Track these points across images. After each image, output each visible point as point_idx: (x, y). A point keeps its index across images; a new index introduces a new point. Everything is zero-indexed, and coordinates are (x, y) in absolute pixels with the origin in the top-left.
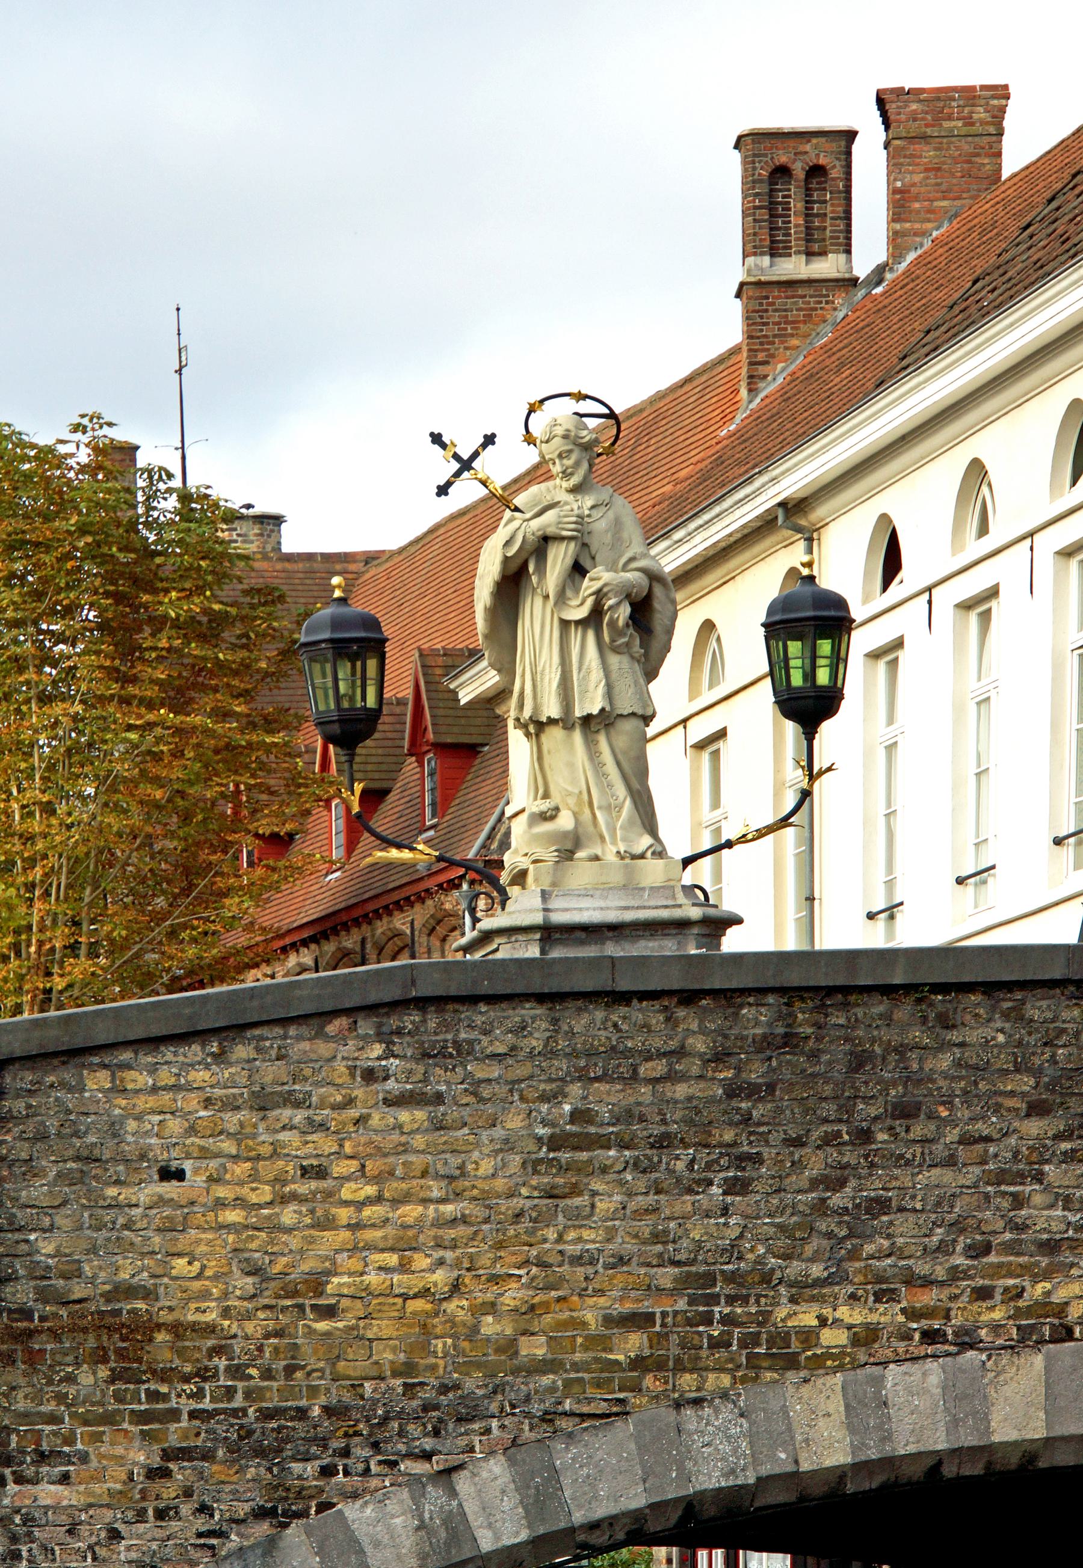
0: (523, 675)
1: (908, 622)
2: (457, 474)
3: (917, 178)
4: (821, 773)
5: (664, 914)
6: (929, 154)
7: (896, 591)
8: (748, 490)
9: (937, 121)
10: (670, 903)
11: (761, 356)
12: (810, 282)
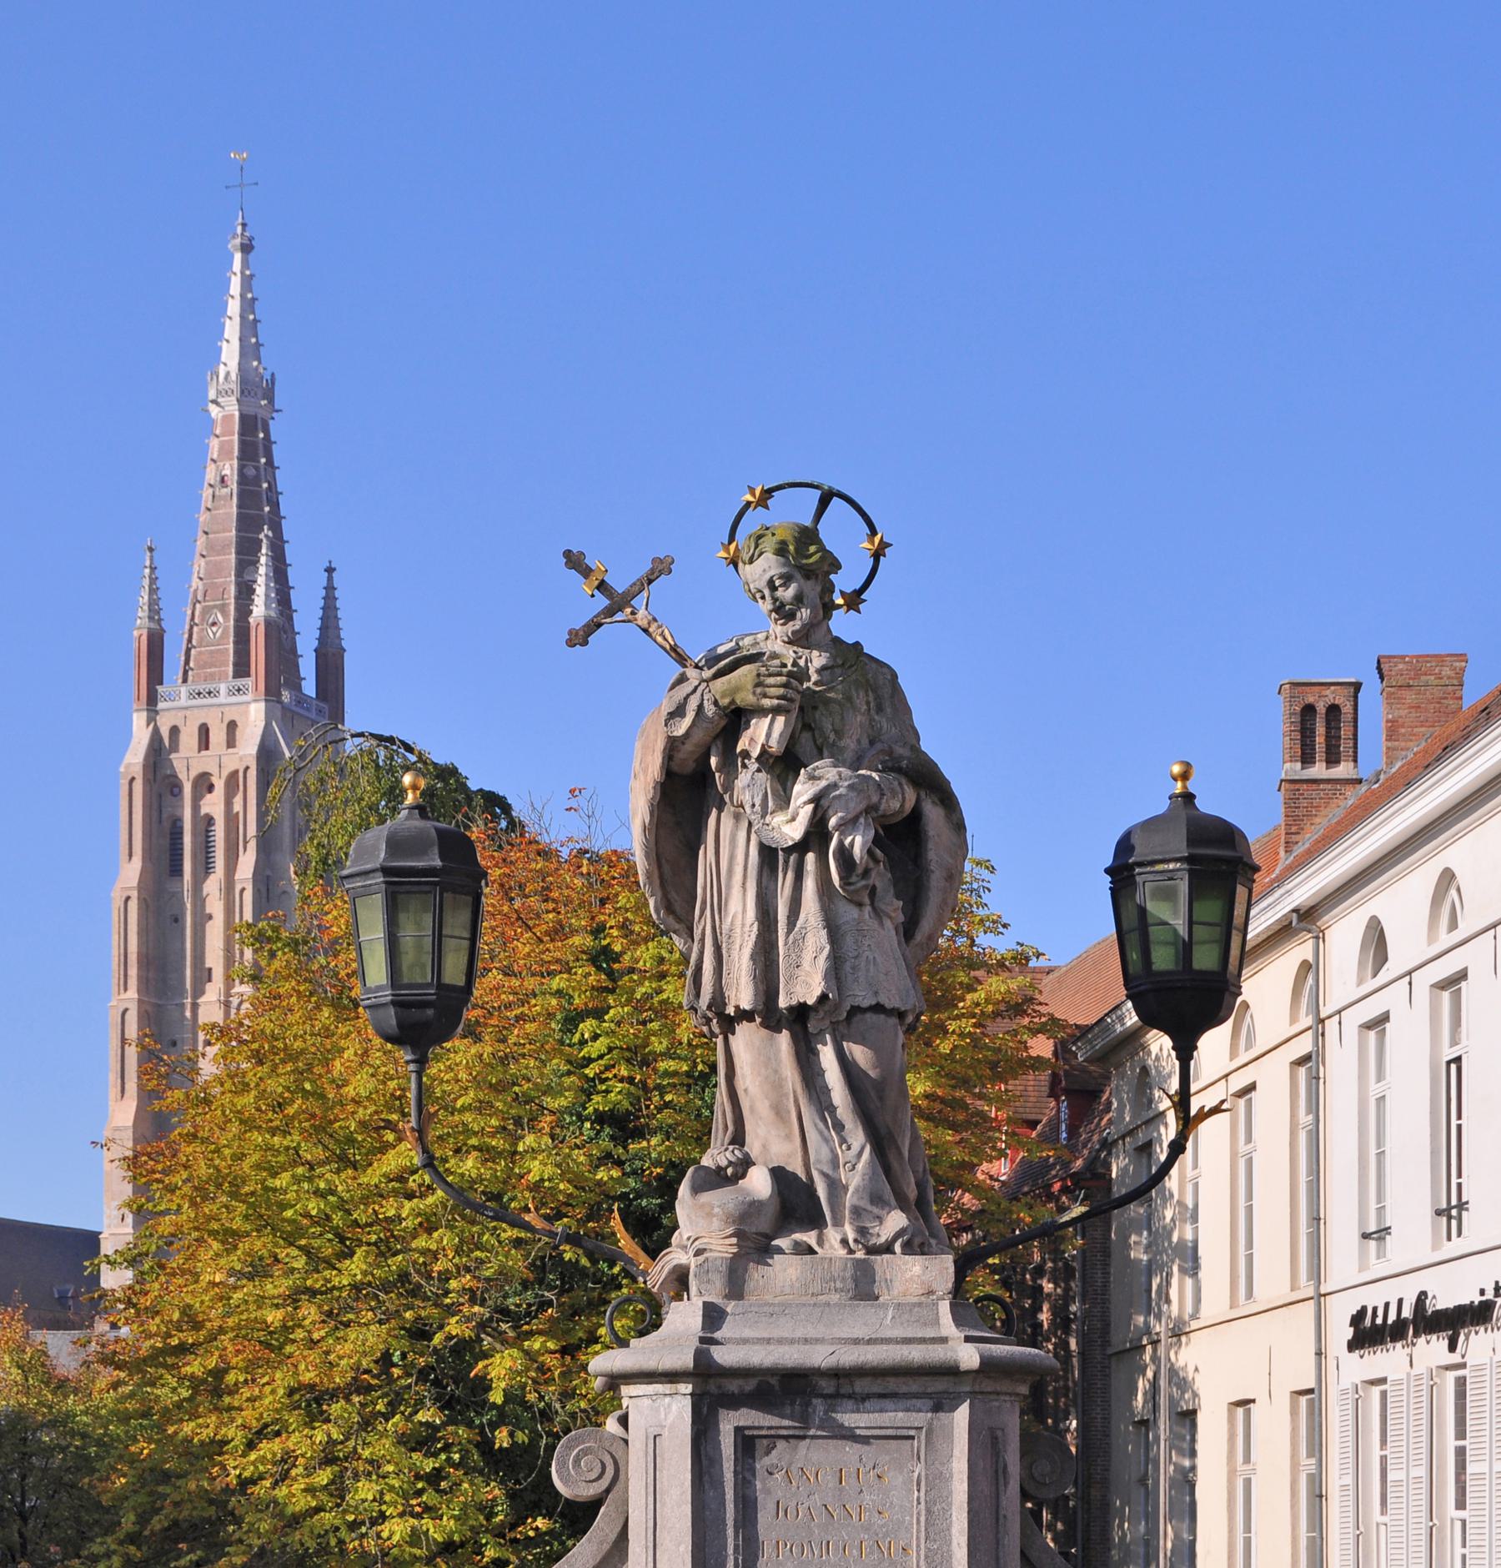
0: (702, 940)
1: (1391, 1000)
2: (610, 612)
3: (1403, 713)
4: (1203, 1115)
5: (916, 1355)
6: (1410, 697)
7: (1384, 976)
8: (1270, 900)
9: (1417, 676)
10: (930, 1333)
11: (1294, 829)
12: (1328, 781)
